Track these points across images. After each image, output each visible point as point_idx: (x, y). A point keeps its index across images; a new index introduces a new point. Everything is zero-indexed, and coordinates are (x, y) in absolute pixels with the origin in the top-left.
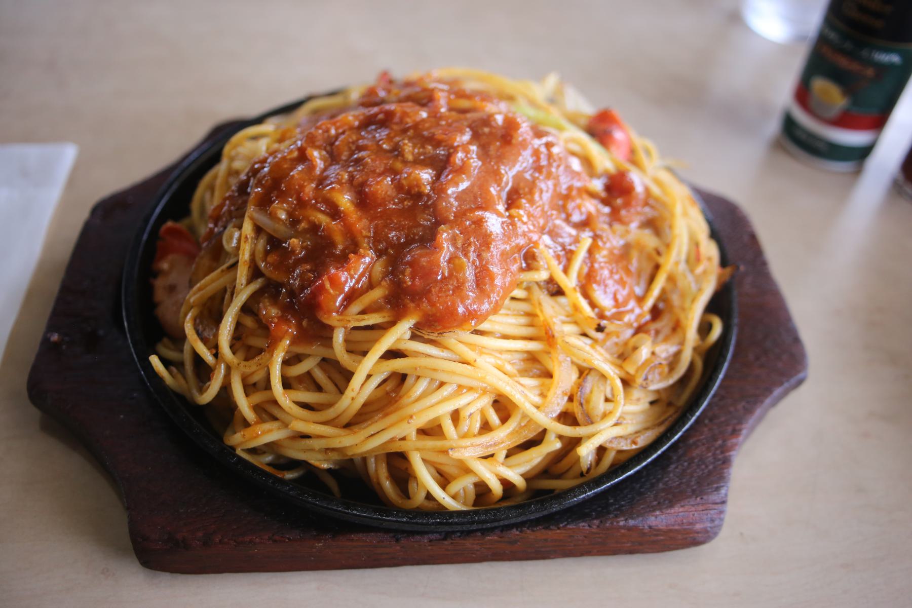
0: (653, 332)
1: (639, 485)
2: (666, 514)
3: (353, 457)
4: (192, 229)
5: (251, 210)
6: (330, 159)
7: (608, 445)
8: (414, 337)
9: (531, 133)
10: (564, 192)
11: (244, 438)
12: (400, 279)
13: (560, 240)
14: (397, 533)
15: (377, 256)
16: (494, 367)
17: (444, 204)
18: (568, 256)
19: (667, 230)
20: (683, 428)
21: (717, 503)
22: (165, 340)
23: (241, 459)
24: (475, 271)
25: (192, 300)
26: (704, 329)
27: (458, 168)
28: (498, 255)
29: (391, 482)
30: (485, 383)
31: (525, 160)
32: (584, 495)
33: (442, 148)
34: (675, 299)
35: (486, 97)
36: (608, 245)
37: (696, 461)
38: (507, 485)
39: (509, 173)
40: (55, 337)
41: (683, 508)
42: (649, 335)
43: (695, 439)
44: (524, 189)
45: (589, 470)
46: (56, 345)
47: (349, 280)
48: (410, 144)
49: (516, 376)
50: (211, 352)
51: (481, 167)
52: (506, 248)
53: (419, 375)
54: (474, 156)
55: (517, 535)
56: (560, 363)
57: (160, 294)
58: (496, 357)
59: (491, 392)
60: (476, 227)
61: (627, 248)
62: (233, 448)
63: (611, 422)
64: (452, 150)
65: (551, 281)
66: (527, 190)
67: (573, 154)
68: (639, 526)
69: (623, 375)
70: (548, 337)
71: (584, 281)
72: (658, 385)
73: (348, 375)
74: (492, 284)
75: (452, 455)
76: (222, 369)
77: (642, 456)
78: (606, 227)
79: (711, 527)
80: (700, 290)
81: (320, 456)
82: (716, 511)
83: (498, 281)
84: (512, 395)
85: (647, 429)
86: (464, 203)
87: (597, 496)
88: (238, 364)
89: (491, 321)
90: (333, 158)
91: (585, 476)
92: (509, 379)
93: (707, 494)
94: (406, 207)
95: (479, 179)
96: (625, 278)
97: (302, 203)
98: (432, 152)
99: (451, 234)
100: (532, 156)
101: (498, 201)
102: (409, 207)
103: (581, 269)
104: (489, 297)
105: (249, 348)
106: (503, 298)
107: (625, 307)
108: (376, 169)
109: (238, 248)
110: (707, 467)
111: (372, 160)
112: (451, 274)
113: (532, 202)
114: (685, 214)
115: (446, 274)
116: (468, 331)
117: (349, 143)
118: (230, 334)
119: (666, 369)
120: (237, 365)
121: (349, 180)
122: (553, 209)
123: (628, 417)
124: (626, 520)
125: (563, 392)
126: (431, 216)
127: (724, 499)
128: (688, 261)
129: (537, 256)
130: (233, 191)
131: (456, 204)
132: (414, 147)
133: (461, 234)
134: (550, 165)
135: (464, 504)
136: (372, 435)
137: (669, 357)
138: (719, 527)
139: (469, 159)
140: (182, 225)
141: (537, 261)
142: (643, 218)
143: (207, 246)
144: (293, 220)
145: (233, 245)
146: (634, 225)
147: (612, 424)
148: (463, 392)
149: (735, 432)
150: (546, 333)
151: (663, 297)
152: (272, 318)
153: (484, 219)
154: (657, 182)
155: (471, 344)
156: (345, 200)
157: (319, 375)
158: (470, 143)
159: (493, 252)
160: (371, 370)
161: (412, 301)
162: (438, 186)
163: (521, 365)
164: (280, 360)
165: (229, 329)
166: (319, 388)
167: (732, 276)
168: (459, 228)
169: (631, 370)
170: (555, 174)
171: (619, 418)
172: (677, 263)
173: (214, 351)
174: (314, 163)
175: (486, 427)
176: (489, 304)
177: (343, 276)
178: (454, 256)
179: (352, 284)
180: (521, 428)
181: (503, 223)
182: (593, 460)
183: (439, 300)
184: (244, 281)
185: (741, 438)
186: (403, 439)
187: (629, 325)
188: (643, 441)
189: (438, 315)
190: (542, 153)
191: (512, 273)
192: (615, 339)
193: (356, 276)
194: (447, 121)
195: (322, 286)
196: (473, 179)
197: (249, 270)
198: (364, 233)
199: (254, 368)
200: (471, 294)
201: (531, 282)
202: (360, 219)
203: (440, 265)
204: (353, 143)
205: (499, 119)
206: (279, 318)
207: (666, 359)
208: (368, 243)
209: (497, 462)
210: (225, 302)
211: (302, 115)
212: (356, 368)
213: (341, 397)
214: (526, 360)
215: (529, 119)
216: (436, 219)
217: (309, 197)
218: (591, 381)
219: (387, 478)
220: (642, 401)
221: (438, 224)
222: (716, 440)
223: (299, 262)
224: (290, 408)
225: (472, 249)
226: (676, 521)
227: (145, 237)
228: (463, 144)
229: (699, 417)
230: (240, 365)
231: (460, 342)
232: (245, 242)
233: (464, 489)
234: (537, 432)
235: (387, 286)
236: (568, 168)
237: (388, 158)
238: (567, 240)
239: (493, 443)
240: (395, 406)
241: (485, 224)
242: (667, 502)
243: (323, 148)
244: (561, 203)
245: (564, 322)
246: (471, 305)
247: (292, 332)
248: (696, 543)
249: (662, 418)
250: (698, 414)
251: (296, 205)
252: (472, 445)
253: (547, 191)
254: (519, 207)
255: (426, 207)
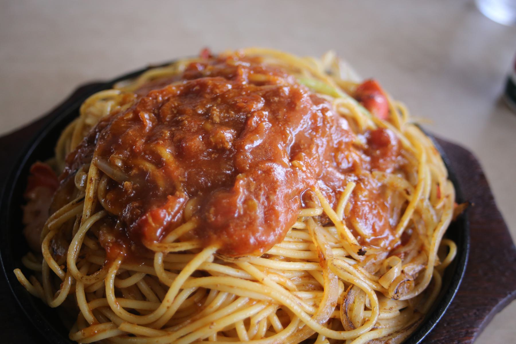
0: (403, 255)
4: (55, 168)
8: (216, 260)
10: (335, 146)
13: (332, 184)
15: (189, 197)
16: (278, 283)
17: (242, 157)
22: (30, 254)
24: (264, 210)
25: (49, 226)
26: (443, 251)
27: (254, 129)
28: (282, 197)
33: (241, 114)
34: (420, 228)
35: (278, 71)
44: (304, 145)
48: (218, 110)
49: (295, 291)
51: (271, 128)
52: (289, 192)
57: (28, 218)
58: (279, 275)
59: (275, 304)
60: (265, 175)
61: (384, 188)
63: (368, 328)
64: (249, 115)
65: (324, 215)
66: (306, 145)
67: (344, 116)
73: (166, 289)
74: (278, 221)
76: (69, 281)
78: (368, 172)
80: (440, 221)
86: (257, 156)
88: (82, 278)
89: (276, 247)
90: (159, 119)
97: (134, 154)
99: (246, 181)
100: (311, 119)
101: (284, 155)
103: (347, 206)
104: (274, 231)
105: (91, 264)
107: (381, 235)
108: (191, 129)
109: (85, 187)
111: (189, 122)
113: (310, 155)
117: (172, 107)
119: (413, 284)
120: (80, 279)
121: (170, 137)
123: (383, 323)
125: (331, 304)
126: (231, 166)
128: (430, 199)
130: (84, 142)
131: (251, 157)
132: (221, 112)
133: (254, 181)
139: (262, 122)
140: (46, 165)
141: (313, 201)
142: (396, 165)
144: (127, 167)
146: (389, 171)
150: (319, 257)
151: (411, 225)
152: (108, 243)
154: (408, 136)
155: (260, 266)
157: (144, 287)
158: (264, 109)
161: (215, 233)
162: (238, 147)
163: (299, 281)
164: (113, 276)
165: (75, 250)
166: (143, 298)
167: (465, 211)
168: (252, 176)
171: (377, 323)
172: (422, 201)
174: (145, 123)
175: (271, 330)
177: (162, 213)
180: (299, 331)
181: (287, 172)
184: (88, 213)
187: (385, 249)
190: (318, 117)
191: (293, 210)
192: (373, 260)
193: (173, 213)
194: (246, 92)
195: (146, 220)
197: (92, 205)
198: (180, 178)
199: (93, 281)
201: (308, 217)
202: (177, 168)
204: (175, 107)
205: (286, 90)
206: (112, 243)
207: (413, 276)
208: (183, 187)
211: (143, 80)
212: (171, 283)
214: (302, 277)
215: (310, 88)
216: (235, 169)
217: (140, 150)
218: (353, 295)
220: (394, 310)
221: (237, 172)
223: (130, 200)
224: (120, 313)
225: (262, 193)
227: (18, 173)
228: (258, 110)
229: (438, 324)
230: (83, 278)
232: (90, 183)
236: (339, 126)
237: (201, 121)
238: (337, 184)
241: (273, 173)
243: (152, 111)
244: (333, 154)
245: (333, 248)
246: (260, 237)
247: (123, 254)
254: (299, 159)
255: (228, 159)
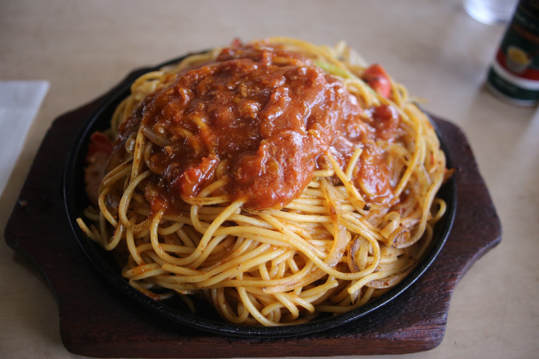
0: (401, 211)
1: (389, 311)
2: (406, 330)
3: (202, 289)
5: (143, 128)
6: (193, 95)
7: (369, 285)
8: (243, 213)
9: (325, 80)
10: (345, 118)
11: (133, 274)
12: (234, 175)
13: (342, 150)
14: (229, 338)
17: (265, 125)
18: (347, 159)
19: (412, 144)
20: (419, 275)
21: (439, 324)
22: (90, 207)
23: (131, 288)
24: (284, 170)
25: (105, 183)
26: (435, 208)
27: (276, 102)
29: (227, 306)
30: (288, 244)
31: (320, 98)
32: (352, 319)
33: (265, 89)
34: (416, 189)
35: (297, 55)
36: (373, 153)
37: (427, 295)
38: (301, 309)
39: (309, 107)
40: (22, 203)
41: (417, 327)
42: (399, 213)
43: (427, 281)
44: (319, 116)
45: (356, 301)
47: (201, 175)
48: (245, 86)
49: (309, 239)
50: (114, 218)
53: (245, 237)
54: (287, 94)
55: (308, 341)
56: (339, 231)
57: (89, 178)
58: (296, 226)
60: (285, 141)
61: (386, 155)
62: (127, 280)
63: (371, 271)
65: (335, 176)
66: (320, 117)
67: (353, 94)
68: (388, 338)
69: (380, 238)
70: (331, 213)
71: (357, 177)
72: (403, 245)
73: (200, 236)
74: (295, 180)
75: (265, 292)
76: (121, 229)
77: (391, 294)
78: (372, 141)
79: (435, 340)
80: (433, 183)
81: (181, 287)
82: (439, 329)
83: (299, 178)
84: (306, 252)
85: (395, 274)
87: (360, 319)
89: (294, 202)
90: (195, 94)
91: (353, 305)
92: (305, 241)
93: (434, 318)
94: (241, 127)
95: (289, 110)
96: (384, 175)
97: (174, 123)
98: (259, 91)
100: (325, 95)
102: (243, 127)
103: (355, 169)
104: (292, 188)
106: (302, 188)
107: (383, 194)
109: (133, 151)
110: (434, 299)
111: (221, 96)
112: (268, 172)
113: (323, 125)
114: (424, 133)
115: (265, 172)
116: (279, 209)
118: (127, 206)
119: (409, 235)
120: (130, 227)
122: (338, 130)
123: (382, 266)
124: (380, 334)
127: (445, 322)
128: (425, 164)
129: (326, 161)
131: (273, 125)
132: (248, 88)
133: (275, 145)
134: (336, 100)
135: (274, 321)
136: (214, 276)
137: (412, 226)
138: (441, 339)
140: (104, 134)
141: (326, 164)
142: (397, 136)
143: (117, 148)
145: (130, 149)
146: (391, 140)
147: (372, 272)
148: (274, 249)
149: (454, 277)
150: (331, 211)
151: (409, 186)
152: (153, 197)
153: (292, 136)
155: (280, 218)
156: (202, 122)
157: (182, 235)
158: (285, 86)
159: (296, 158)
160: (214, 234)
161: (242, 189)
165: (126, 203)
166: (182, 244)
167: (454, 175)
169: (386, 236)
170: (339, 107)
172: (418, 166)
173: (116, 217)
174: (184, 98)
175: (289, 272)
176: (293, 192)
177: (197, 172)
178: (270, 160)
179: (203, 177)
181: (304, 139)
182: (359, 295)
183: (259, 189)
184: (136, 173)
185: (457, 281)
186: (235, 278)
187: (386, 206)
188: (392, 283)
189: (259, 199)
190: (331, 93)
191: (309, 171)
193: (206, 172)
196: (285, 110)
197: (139, 166)
199: (140, 229)
200: (280, 186)
201: (321, 177)
202: (211, 134)
203: (260, 166)
205: (304, 70)
207: (409, 228)
209: (295, 295)
210: (125, 186)
211: (184, 65)
212: (205, 231)
213: (195, 250)
215: (325, 70)
216: (260, 136)
217: (179, 120)
219: (224, 303)
220: (392, 256)
221: (261, 138)
222: (440, 282)
223: (171, 161)
224: (163, 255)
225: (283, 156)
226: (412, 336)
227: (81, 141)
228: (280, 87)
229: (429, 267)
230: (132, 226)
231: (272, 216)
232: (138, 147)
233: (274, 312)
234: (322, 276)
235: (226, 179)
236: (349, 103)
238: (347, 150)
239: (293, 283)
240: (229, 257)
241: (292, 139)
242: (407, 323)
244: (343, 125)
245: (342, 204)
246: (280, 193)
248: (425, 349)
249: (406, 268)
250: (429, 265)
251: (170, 124)
252: (279, 285)
253: (334, 118)
254: (315, 128)
255: (254, 127)
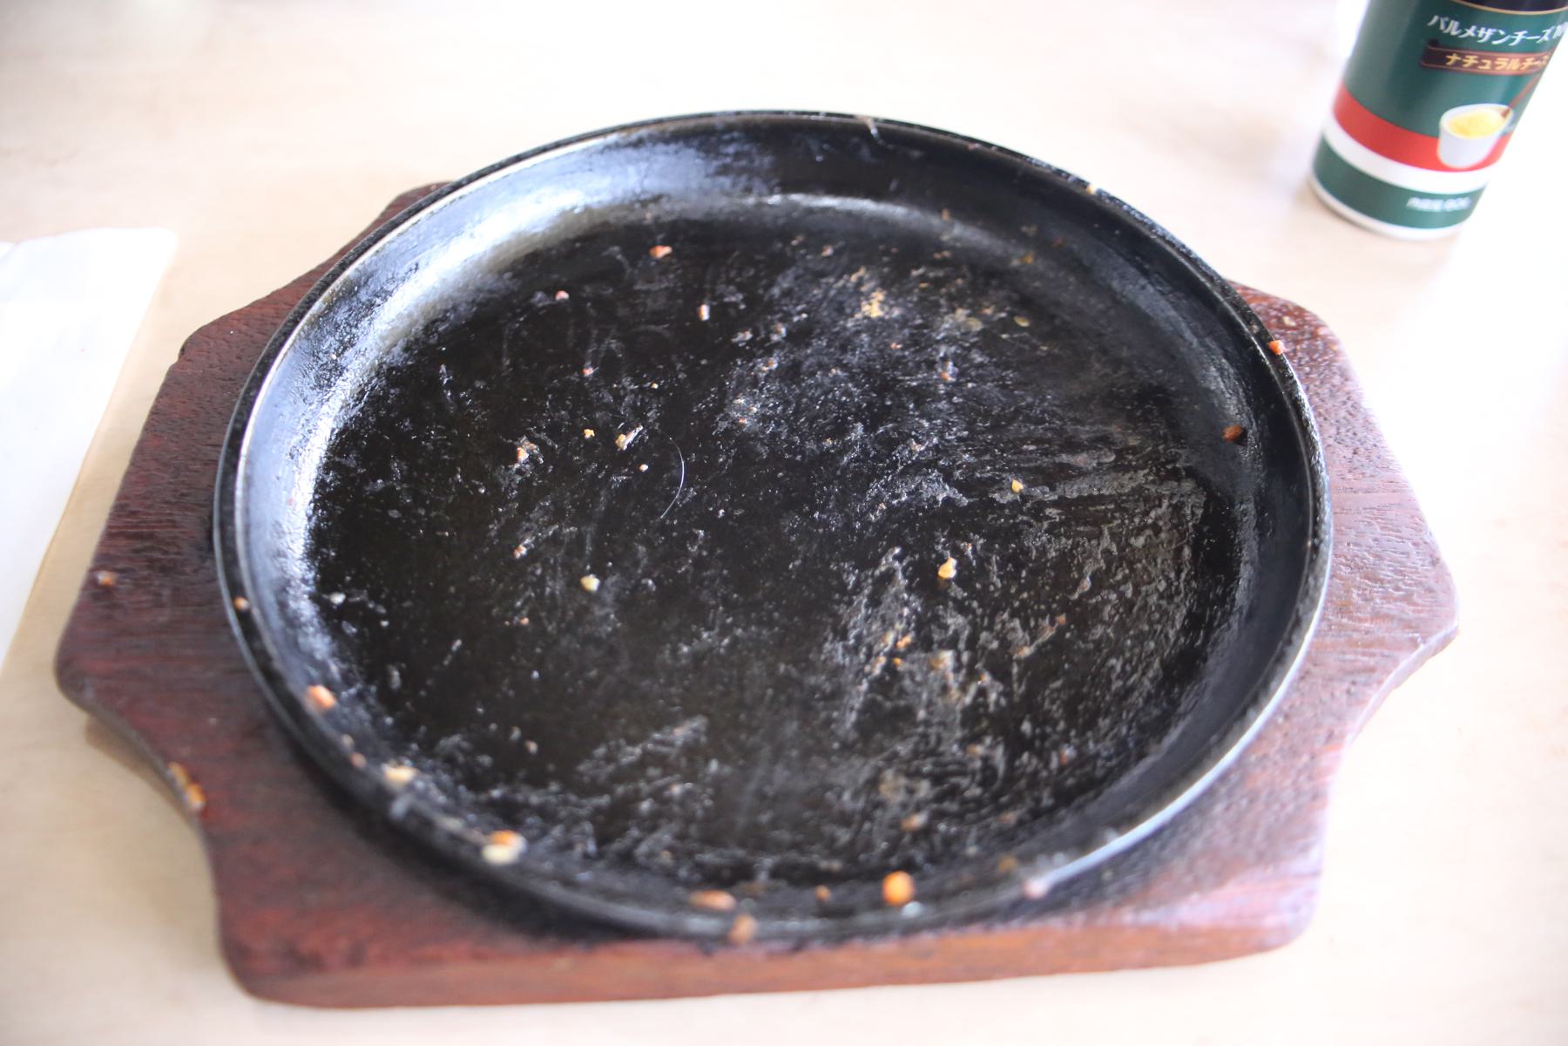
40: (104, 577)
46: (107, 590)
110: (1283, 806)
248: (1262, 948)
